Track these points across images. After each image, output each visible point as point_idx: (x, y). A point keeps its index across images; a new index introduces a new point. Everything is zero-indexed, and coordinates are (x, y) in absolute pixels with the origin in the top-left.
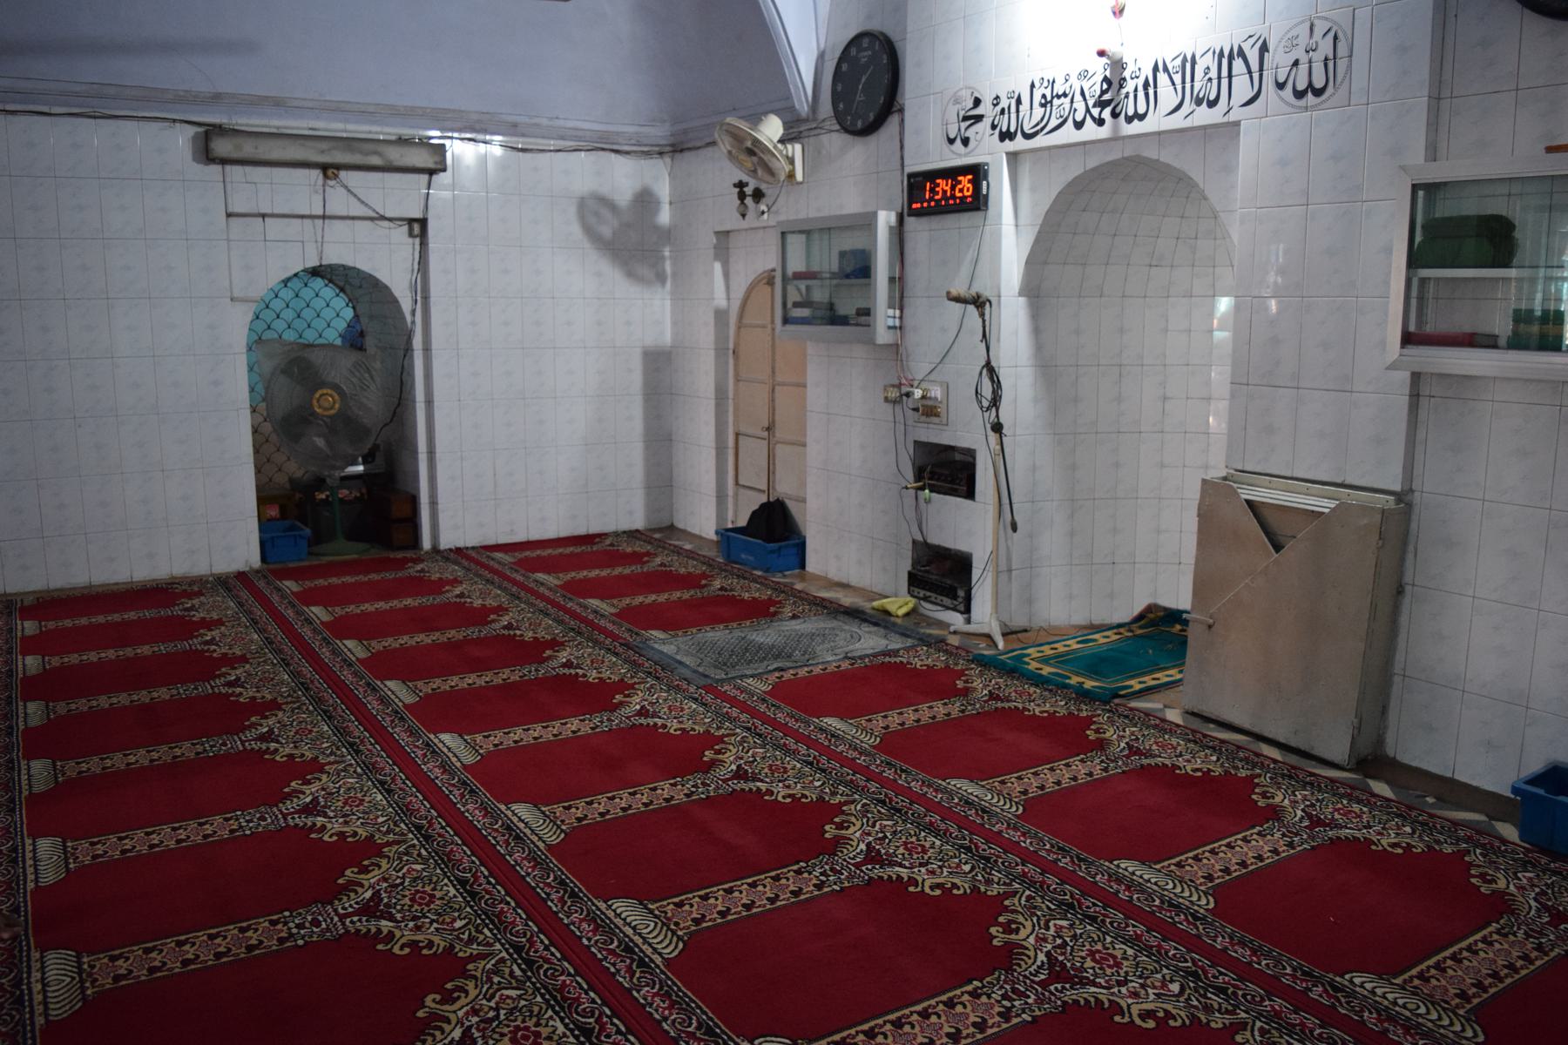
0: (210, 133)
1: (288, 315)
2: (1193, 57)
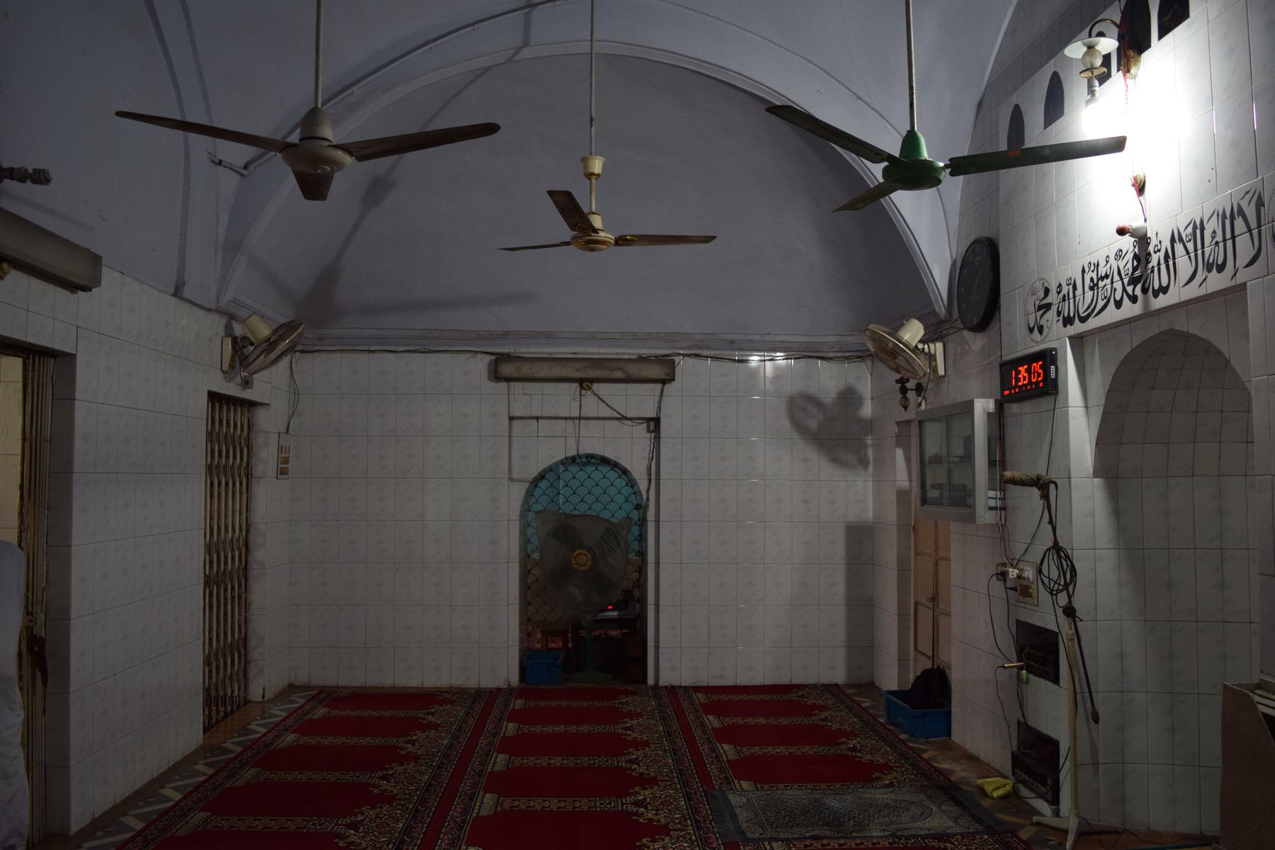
0: (501, 359)
2: (1202, 222)
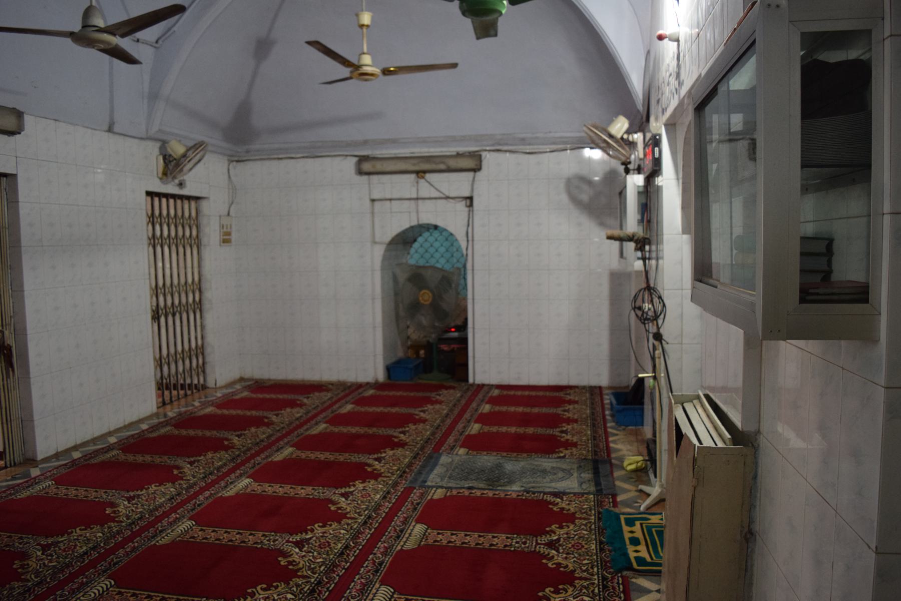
0: (362, 159)
1: (442, 250)
